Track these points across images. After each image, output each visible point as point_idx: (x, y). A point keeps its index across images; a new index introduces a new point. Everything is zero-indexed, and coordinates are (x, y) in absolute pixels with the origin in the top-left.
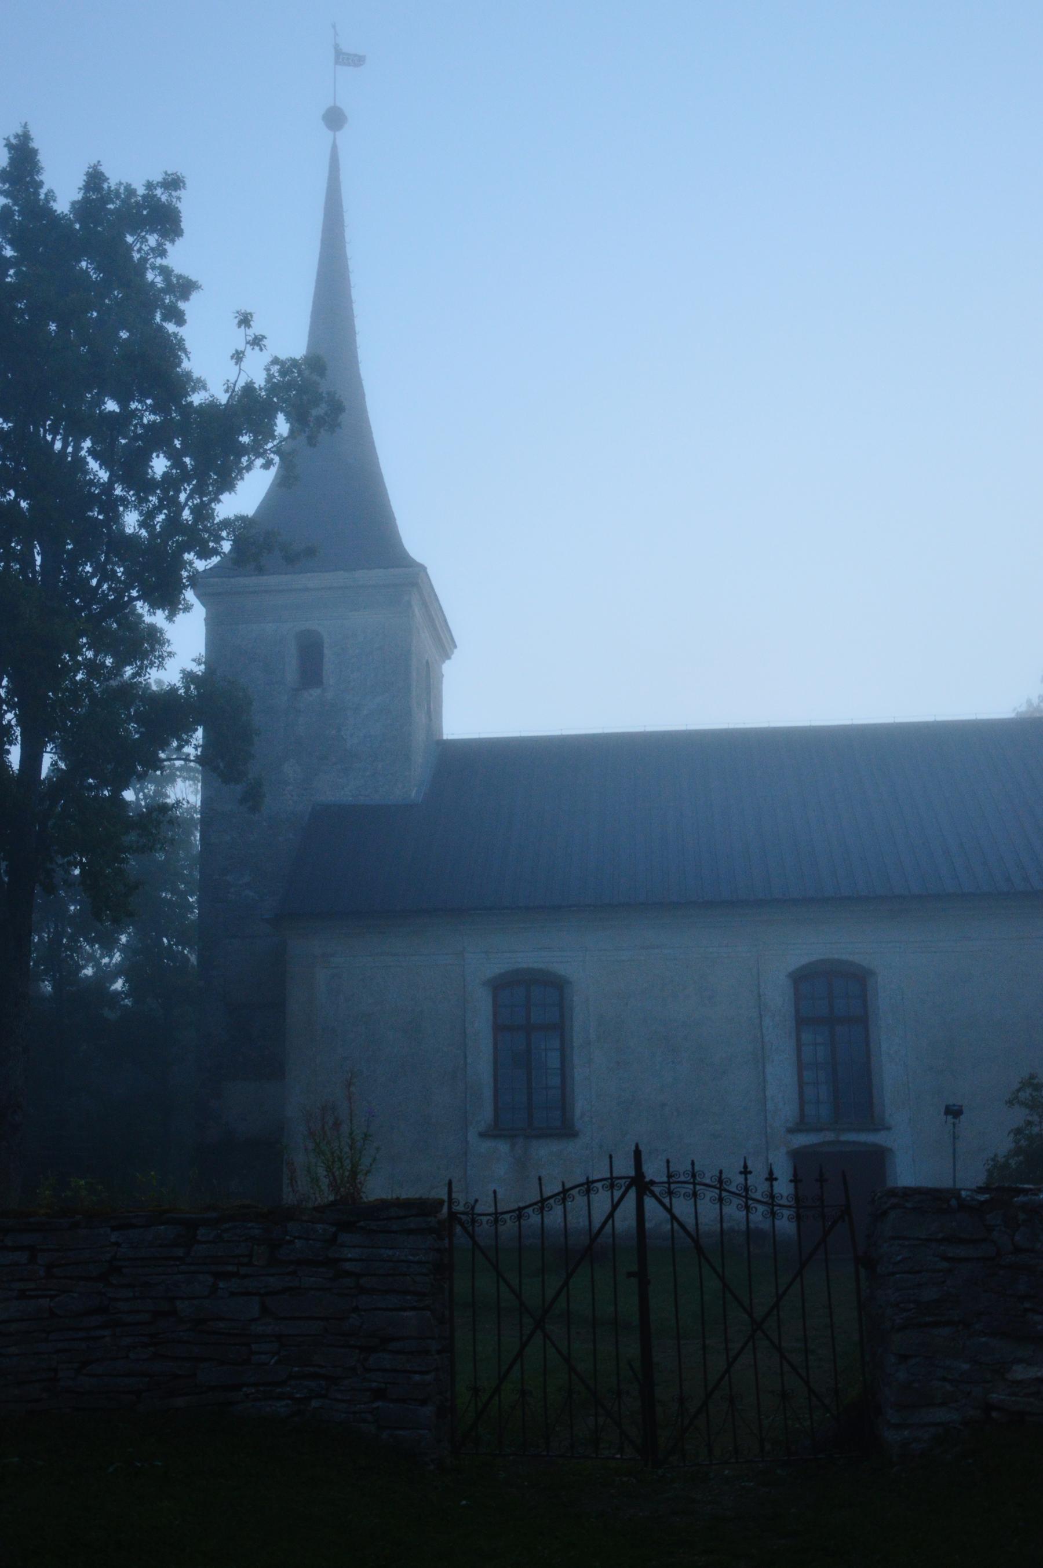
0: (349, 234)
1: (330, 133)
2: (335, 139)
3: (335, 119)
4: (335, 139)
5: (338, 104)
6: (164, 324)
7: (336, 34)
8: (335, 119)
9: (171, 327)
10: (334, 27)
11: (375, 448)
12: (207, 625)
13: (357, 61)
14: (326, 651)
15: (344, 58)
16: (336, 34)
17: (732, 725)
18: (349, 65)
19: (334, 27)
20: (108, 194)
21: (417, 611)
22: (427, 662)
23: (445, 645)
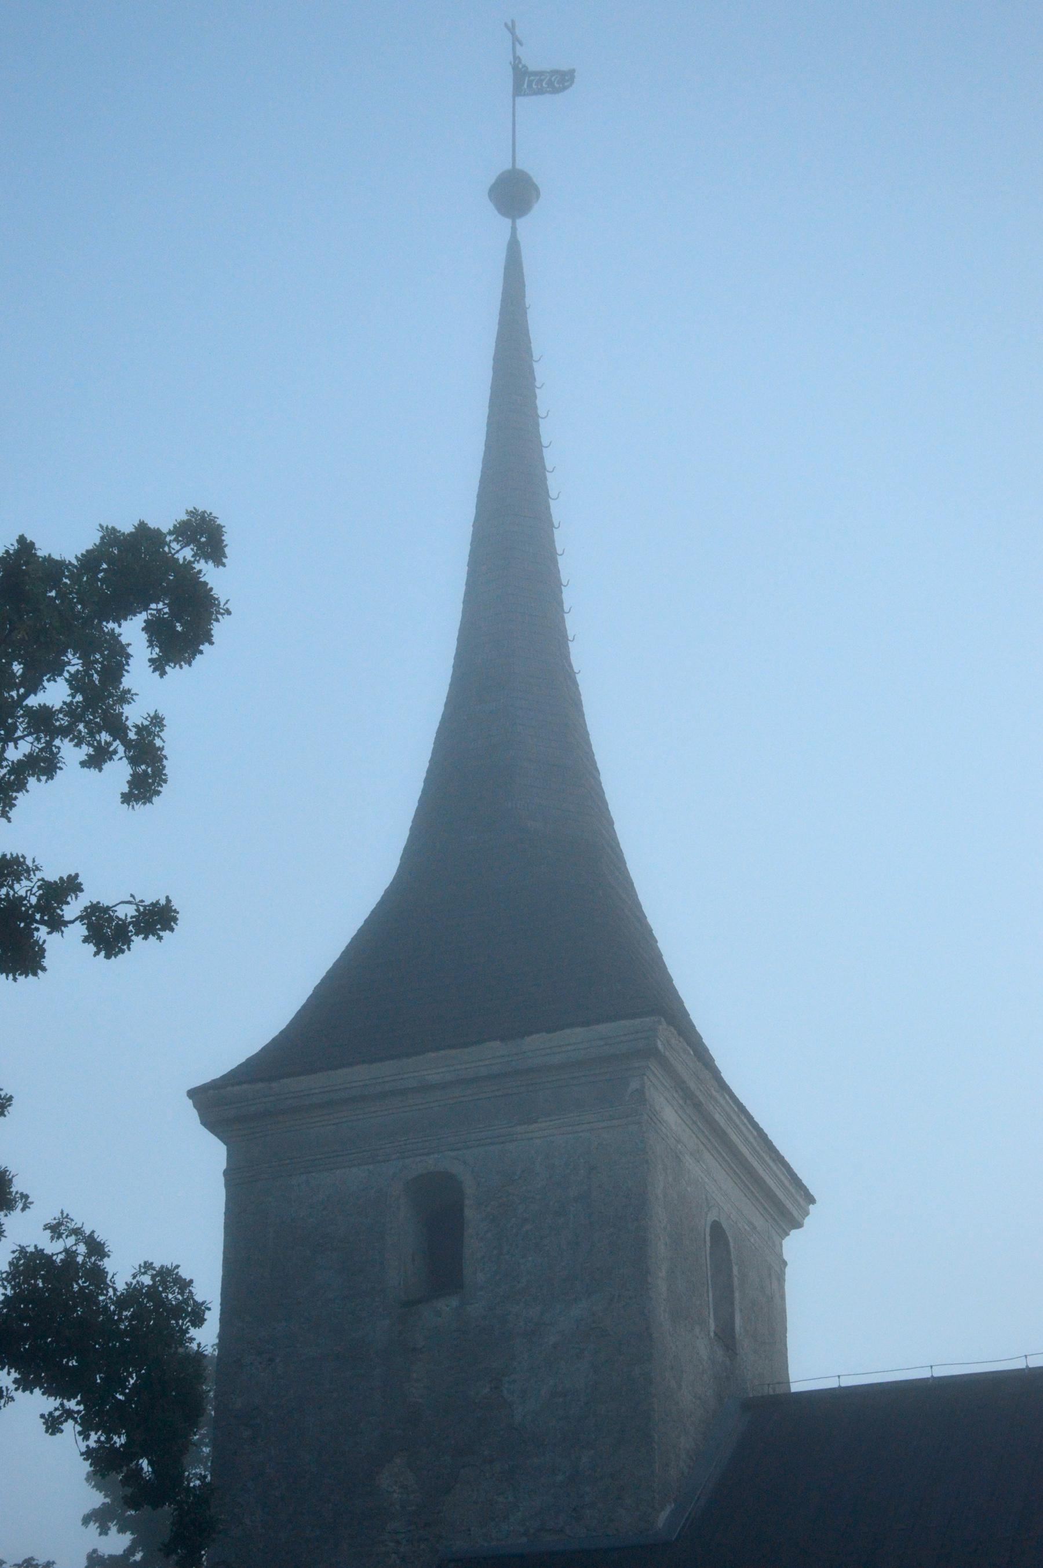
0: (546, 400)
1: (508, 222)
2: (514, 229)
3: (513, 194)
4: (514, 229)
5: (519, 166)
6: (201, 565)
7: (516, 41)
8: (513, 194)
9: (42, 933)
10: (511, 28)
11: (605, 804)
12: (228, 1185)
13: (560, 81)
14: (469, 1213)
15: (527, 82)
16: (516, 41)
17: (328, 965)
18: (540, 92)
19: (511, 28)
20: (62, 885)
21: (670, 1115)
22: (717, 1229)
23: (781, 1198)
